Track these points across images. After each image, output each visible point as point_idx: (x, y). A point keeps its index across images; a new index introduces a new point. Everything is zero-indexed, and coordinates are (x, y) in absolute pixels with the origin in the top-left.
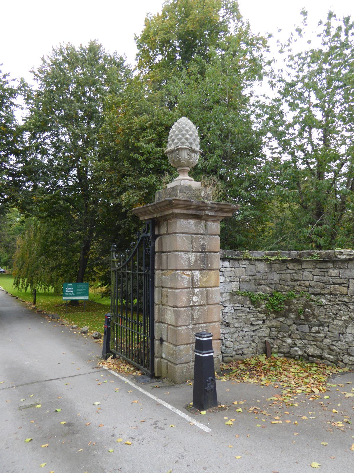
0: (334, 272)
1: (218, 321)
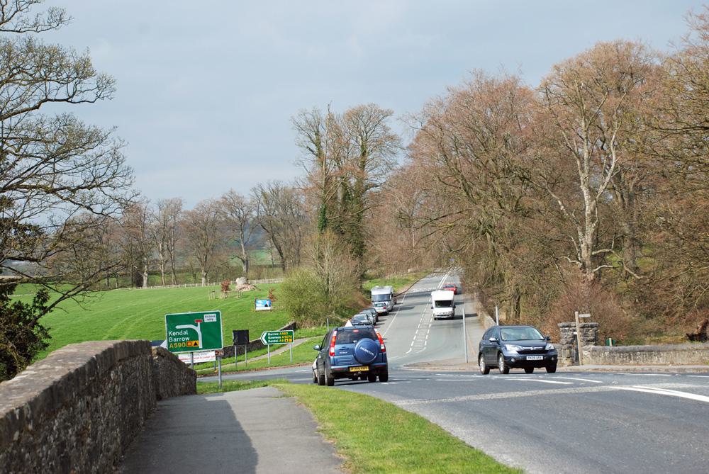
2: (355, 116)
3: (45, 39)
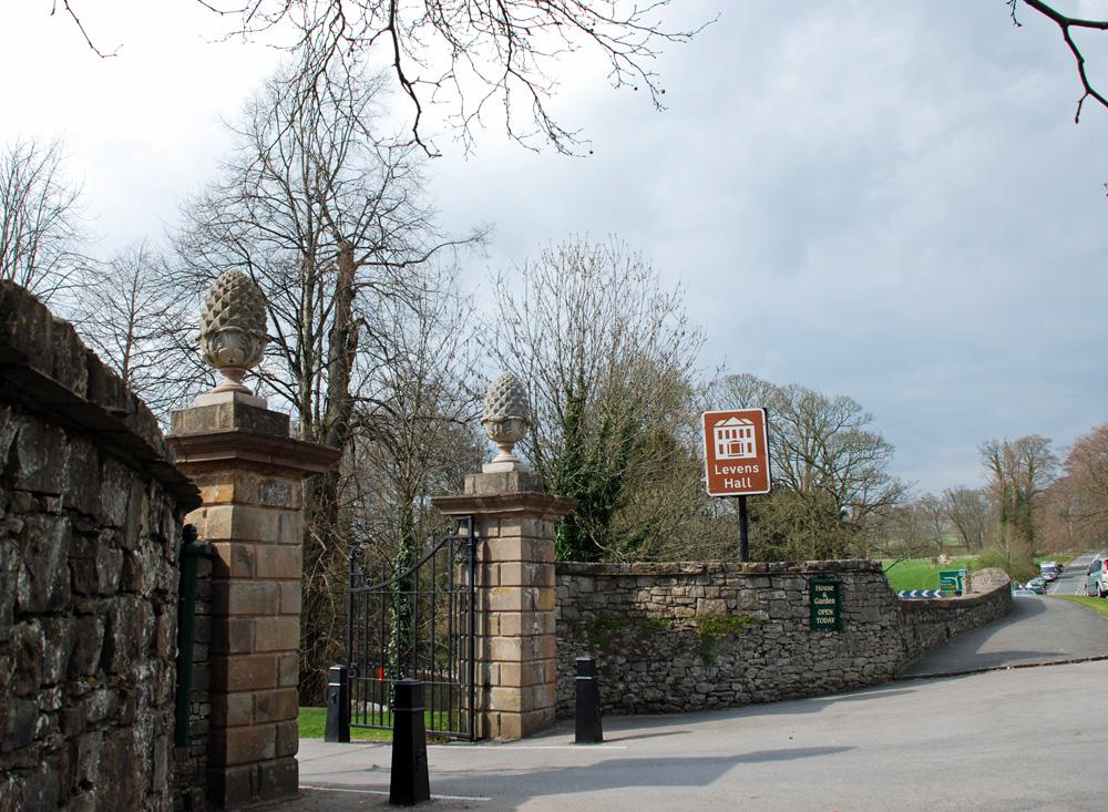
0: (678, 590)
1: (205, 735)
2: (1023, 443)
3: (864, 428)
